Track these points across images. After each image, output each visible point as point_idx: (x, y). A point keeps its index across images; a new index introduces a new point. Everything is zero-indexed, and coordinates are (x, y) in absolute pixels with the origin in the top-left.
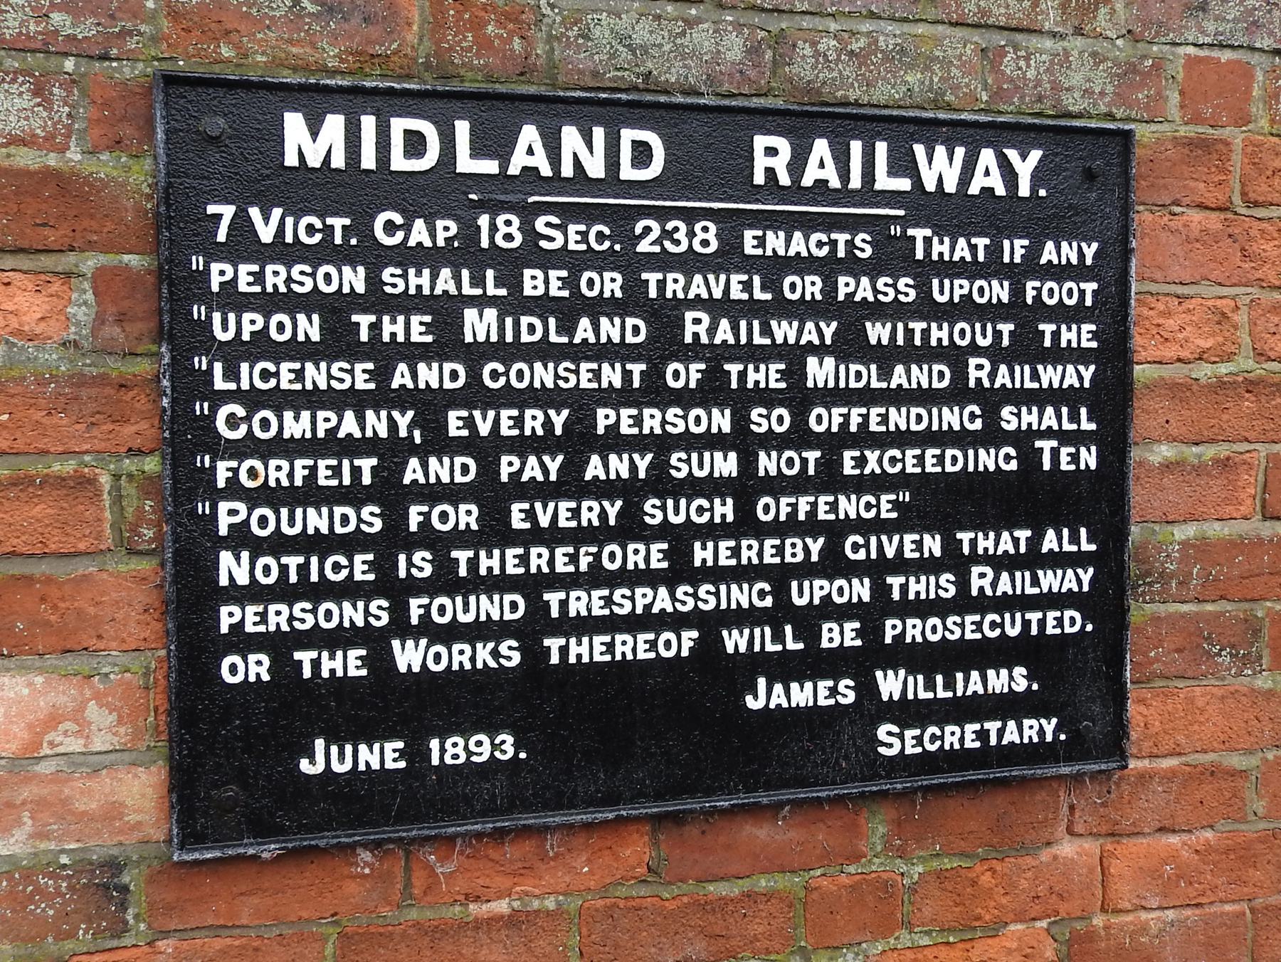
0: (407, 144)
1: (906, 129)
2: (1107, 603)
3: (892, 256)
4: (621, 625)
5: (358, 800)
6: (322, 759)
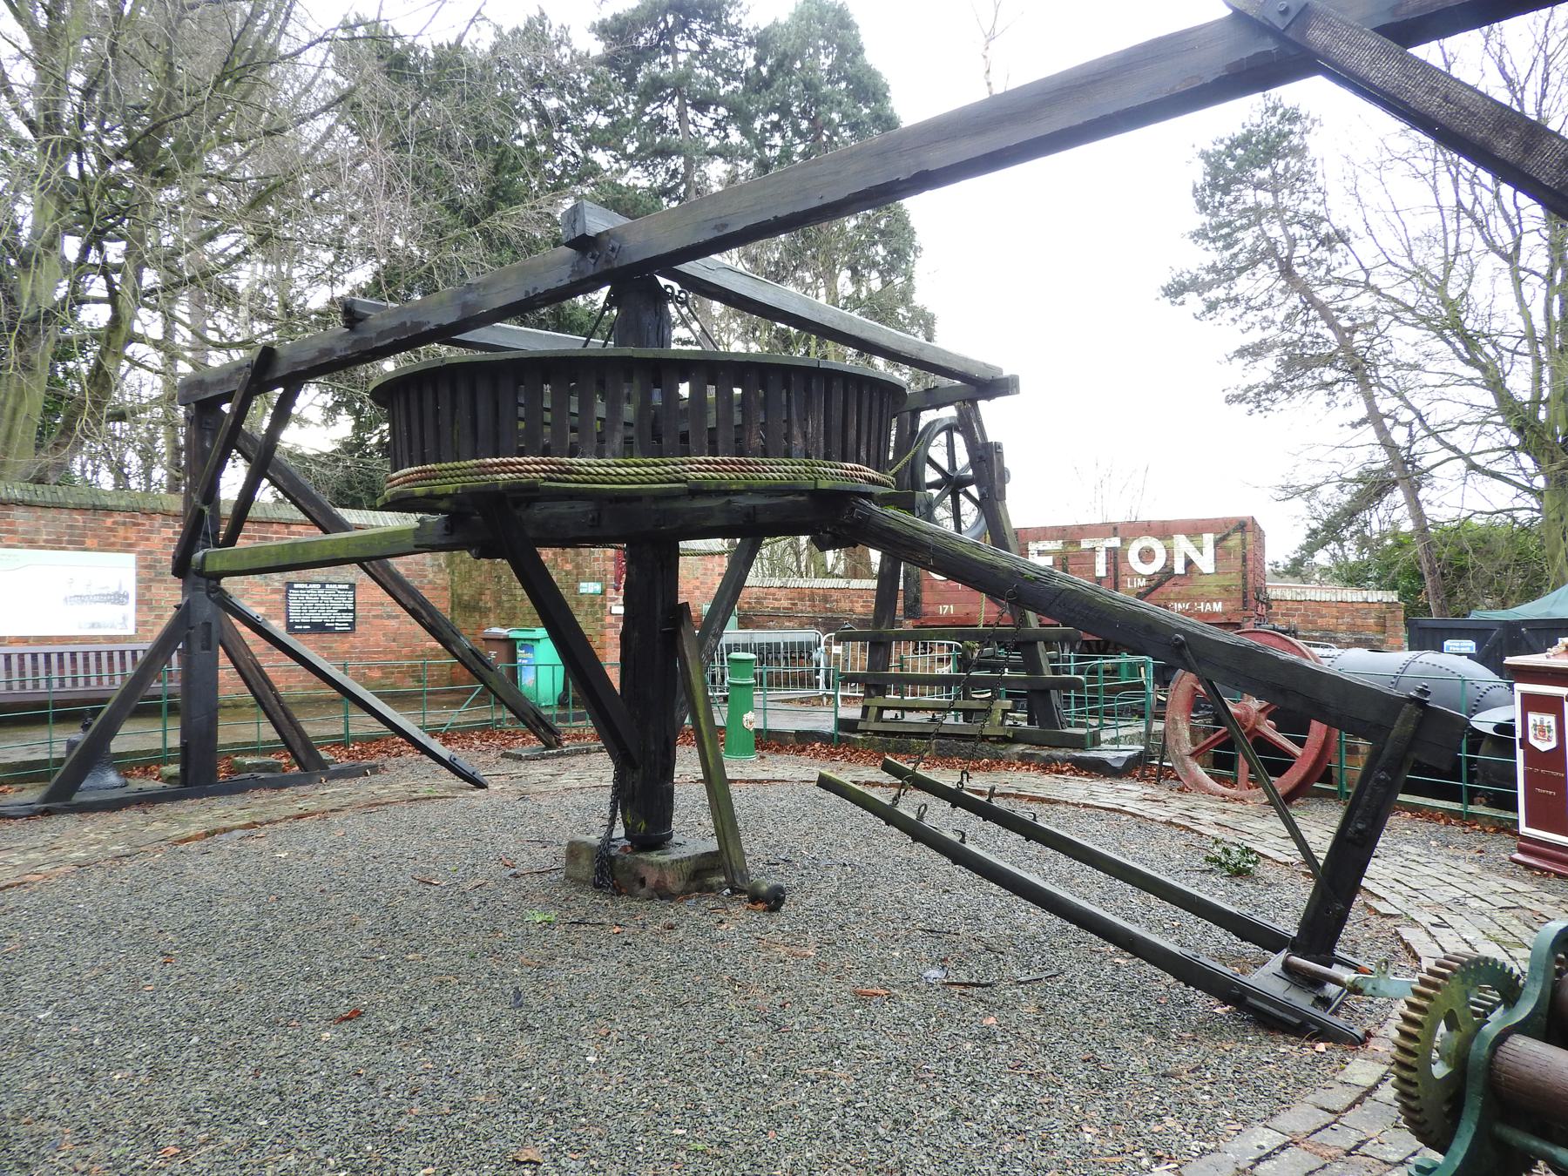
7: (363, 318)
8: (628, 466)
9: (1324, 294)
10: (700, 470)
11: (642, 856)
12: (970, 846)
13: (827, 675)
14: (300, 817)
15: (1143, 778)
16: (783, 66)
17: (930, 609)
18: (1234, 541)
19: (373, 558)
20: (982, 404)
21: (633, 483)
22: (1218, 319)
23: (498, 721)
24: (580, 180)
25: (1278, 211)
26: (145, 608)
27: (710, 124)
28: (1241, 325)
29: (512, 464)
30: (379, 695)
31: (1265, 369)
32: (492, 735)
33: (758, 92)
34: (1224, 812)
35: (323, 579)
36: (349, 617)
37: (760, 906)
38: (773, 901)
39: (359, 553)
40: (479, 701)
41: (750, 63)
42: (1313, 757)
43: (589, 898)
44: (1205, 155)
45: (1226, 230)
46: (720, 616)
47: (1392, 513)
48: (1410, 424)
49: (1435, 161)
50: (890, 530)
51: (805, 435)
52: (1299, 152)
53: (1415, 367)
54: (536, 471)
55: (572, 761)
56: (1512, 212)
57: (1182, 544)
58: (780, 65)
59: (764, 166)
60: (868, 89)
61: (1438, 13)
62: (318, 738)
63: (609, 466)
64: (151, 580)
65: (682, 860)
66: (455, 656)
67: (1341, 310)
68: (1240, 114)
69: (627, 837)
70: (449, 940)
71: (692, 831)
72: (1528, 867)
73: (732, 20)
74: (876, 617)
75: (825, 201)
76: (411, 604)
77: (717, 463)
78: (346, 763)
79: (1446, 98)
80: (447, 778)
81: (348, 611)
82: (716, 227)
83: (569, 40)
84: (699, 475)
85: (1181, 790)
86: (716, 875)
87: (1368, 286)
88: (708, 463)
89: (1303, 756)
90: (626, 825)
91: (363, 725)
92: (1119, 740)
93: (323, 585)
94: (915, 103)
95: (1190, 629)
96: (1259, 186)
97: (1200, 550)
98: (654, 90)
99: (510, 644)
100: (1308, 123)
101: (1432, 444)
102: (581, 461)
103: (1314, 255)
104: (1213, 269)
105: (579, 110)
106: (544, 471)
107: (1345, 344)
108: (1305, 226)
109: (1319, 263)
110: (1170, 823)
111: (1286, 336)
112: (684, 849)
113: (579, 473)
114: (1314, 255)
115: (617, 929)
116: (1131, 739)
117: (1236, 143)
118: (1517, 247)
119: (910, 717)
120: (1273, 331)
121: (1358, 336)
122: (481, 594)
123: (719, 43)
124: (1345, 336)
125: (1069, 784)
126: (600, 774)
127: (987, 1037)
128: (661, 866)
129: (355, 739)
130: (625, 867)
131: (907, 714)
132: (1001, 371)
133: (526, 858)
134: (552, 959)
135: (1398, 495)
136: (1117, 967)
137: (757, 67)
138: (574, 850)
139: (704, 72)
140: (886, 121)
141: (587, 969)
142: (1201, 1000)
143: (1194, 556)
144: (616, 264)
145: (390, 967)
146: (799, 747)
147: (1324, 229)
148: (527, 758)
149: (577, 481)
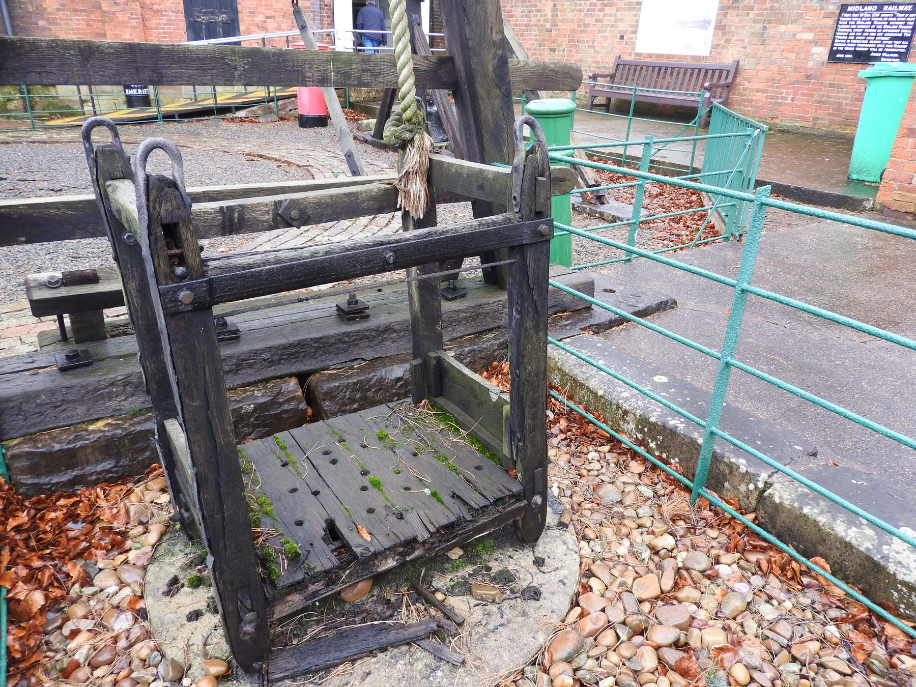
0: (856, 9)
1: (898, 5)
2: (908, 49)
3: (895, 16)
4: (862, 48)
5: (840, 59)
6: (838, 56)
26: (720, 32)
61: (190, 448)
64: (729, 7)
81: (903, 38)
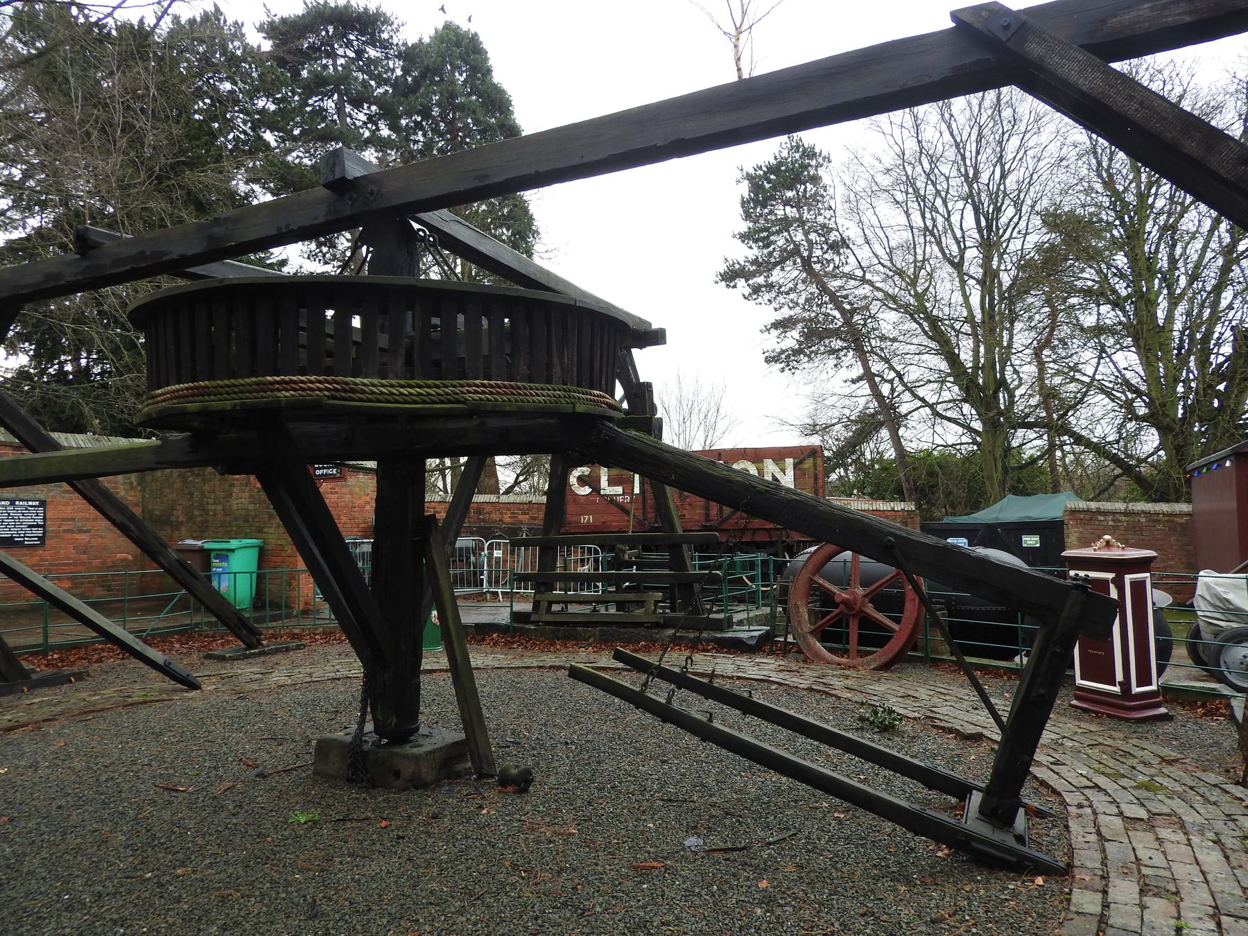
7: (97, 246)
8: (411, 386)
9: (834, 284)
10: (476, 392)
11: (397, 750)
12: (717, 724)
13: (490, 573)
14: (10, 729)
15: (771, 653)
16: (427, 72)
17: (574, 519)
18: (808, 464)
19: (83, 478)
20: (635, 351)
21: (415, 402)
22: (760, 300)
23: (197, 625)
24: (252, 153)
25: (801, 222)
27: (364, 118)
28: (775, 305)
29: (295, 382)
30: (92, 605)
31: (792, 339)
32: (191, 638)
33: (406, 96)
34: (847, 677)
35: (13, 496)
36: (40, 532)
37: (510, 789)
38: (521, 783)
39: (70, 470)
40: (183, 605)
41: (399, 72)
42: (908, 631)
43: (347, 795)
44: (749, 177)
45: (765, 234)
46: (454, 526)
47: (881, 446)
48: (891, 382)
49: (907, 193)
50: (634, 449)
51: (562, 363)
52: (815, 180)
53: (894, 340)
54: (320, 389)
55: (274, 659)
56: (959, 234)
57: (770, 467)
58: (423, 75)
59: (408, 156)
60: (497, 102)
62: (16, 648)
63: (392, 386)
65: (434, 751)
66: (162, 566)
67: (846, 297)
68: (765, 152)
69: (376, 731)
70: (216, 849)
71: (438, 726)
72: (1085, 710)
73: (385, 36)
74: (545, 525)
75: (585, 160)
76: (120, 519)
77: (491, 386)
78: (49, 671)
79: (1141, 104)
80: (158, 682)
81: (38, 526)
82: (477, 178)
83: (243, 35)
84: (476, 397)
85: (805, 661)
86: (468, 762)
87: (864, 280)
88: (483, 385)
89: (900, 631)
90: (374, 719)
91: (65, 631)
92: (747, 622)
93: (12, 503)
94: (534, 115)
95: (898, 532)
96: (787, 203)
97: (783, 471)
98: (319, 85)
99: (205, 554)
100: (820, 160)
101: (907, 396)
102: (365, 381)
103: (826, 256)
104: (755, 262)
105: (252, 95)
106: (328, 389)
107: (848, 322)
108: (819, 235)
109: (828, 262)
110: (810, 690)
111: (806, 315)
112: (433, 741)
113: (363, 392)
114: (826, 256)
115: (384, 824)
116: (758, 621)
117: (772, 169)
118: (962, 258)
119: (573, 608)
120: (798, 310)
121: (856, 318)
122: (173, 509)
123: (372, 53)
124: (847, 315)
125: (718, 660)
126: (308, 670)
127: (768, 901)
128: (417, 758)
129: (54, 648)
130: (374, 763)
131: (569, 606)
132: (650, 324)
133: (266, 757)
134: (329, 860)
135: (884, 433)
136: (840, 822)
137: (404, 76)
138: (324, 748)
139: (360, 76)
140: (511, 130)
141: (372, 868)
142: (922, 844)
143: (779, 476)
144: (374, 207)
145: (161, 885)
146: (479, 638)
147: (833, 236)
148: (232, 659)
149: (361, 400)
